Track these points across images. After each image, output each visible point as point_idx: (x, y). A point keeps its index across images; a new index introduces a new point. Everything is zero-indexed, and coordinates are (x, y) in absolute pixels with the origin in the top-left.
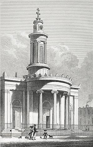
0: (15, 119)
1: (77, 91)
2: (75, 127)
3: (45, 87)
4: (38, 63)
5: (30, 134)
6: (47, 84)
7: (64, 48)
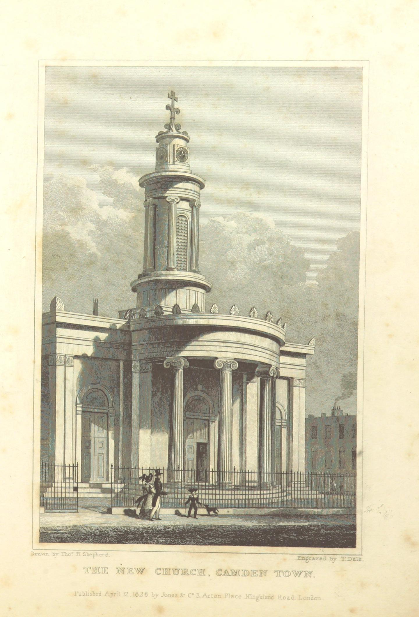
0: (92, 451)
1: (301, 361)
2: (295, 478)
3: (195, 350)
4: (172, 269)
5: (139, 500)
6: (175, 186)
7: (259, 221)
